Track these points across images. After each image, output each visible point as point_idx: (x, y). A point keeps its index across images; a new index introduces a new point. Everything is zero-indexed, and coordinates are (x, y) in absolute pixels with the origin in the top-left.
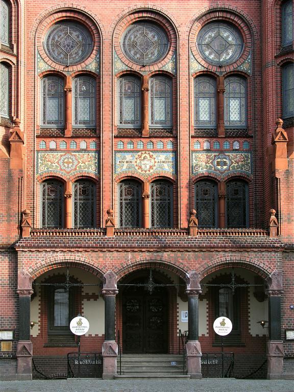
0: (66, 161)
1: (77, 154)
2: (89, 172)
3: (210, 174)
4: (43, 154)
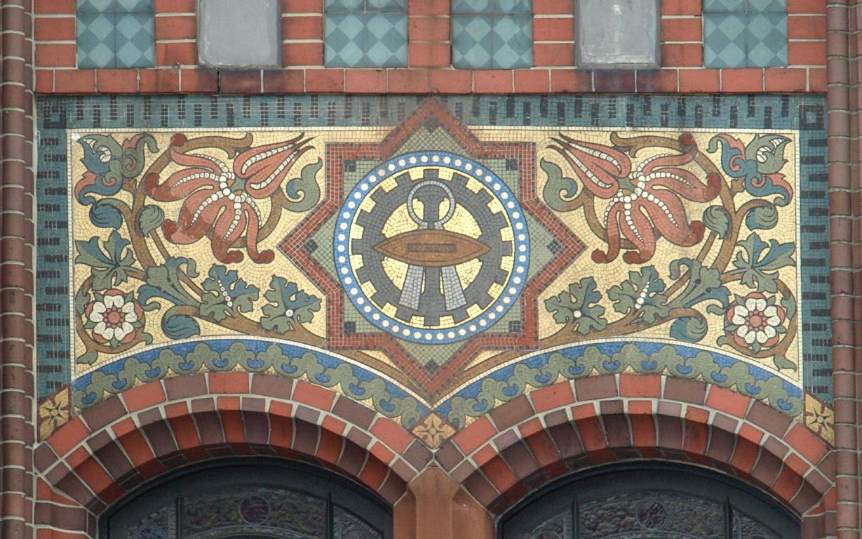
0: (399, 223)
1: (538, 135)
2: (702, 369)
4: (122, 134)
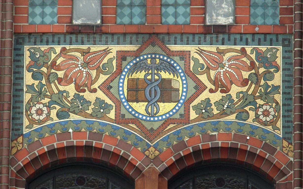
1: (192, 49)
3: (98, 136)
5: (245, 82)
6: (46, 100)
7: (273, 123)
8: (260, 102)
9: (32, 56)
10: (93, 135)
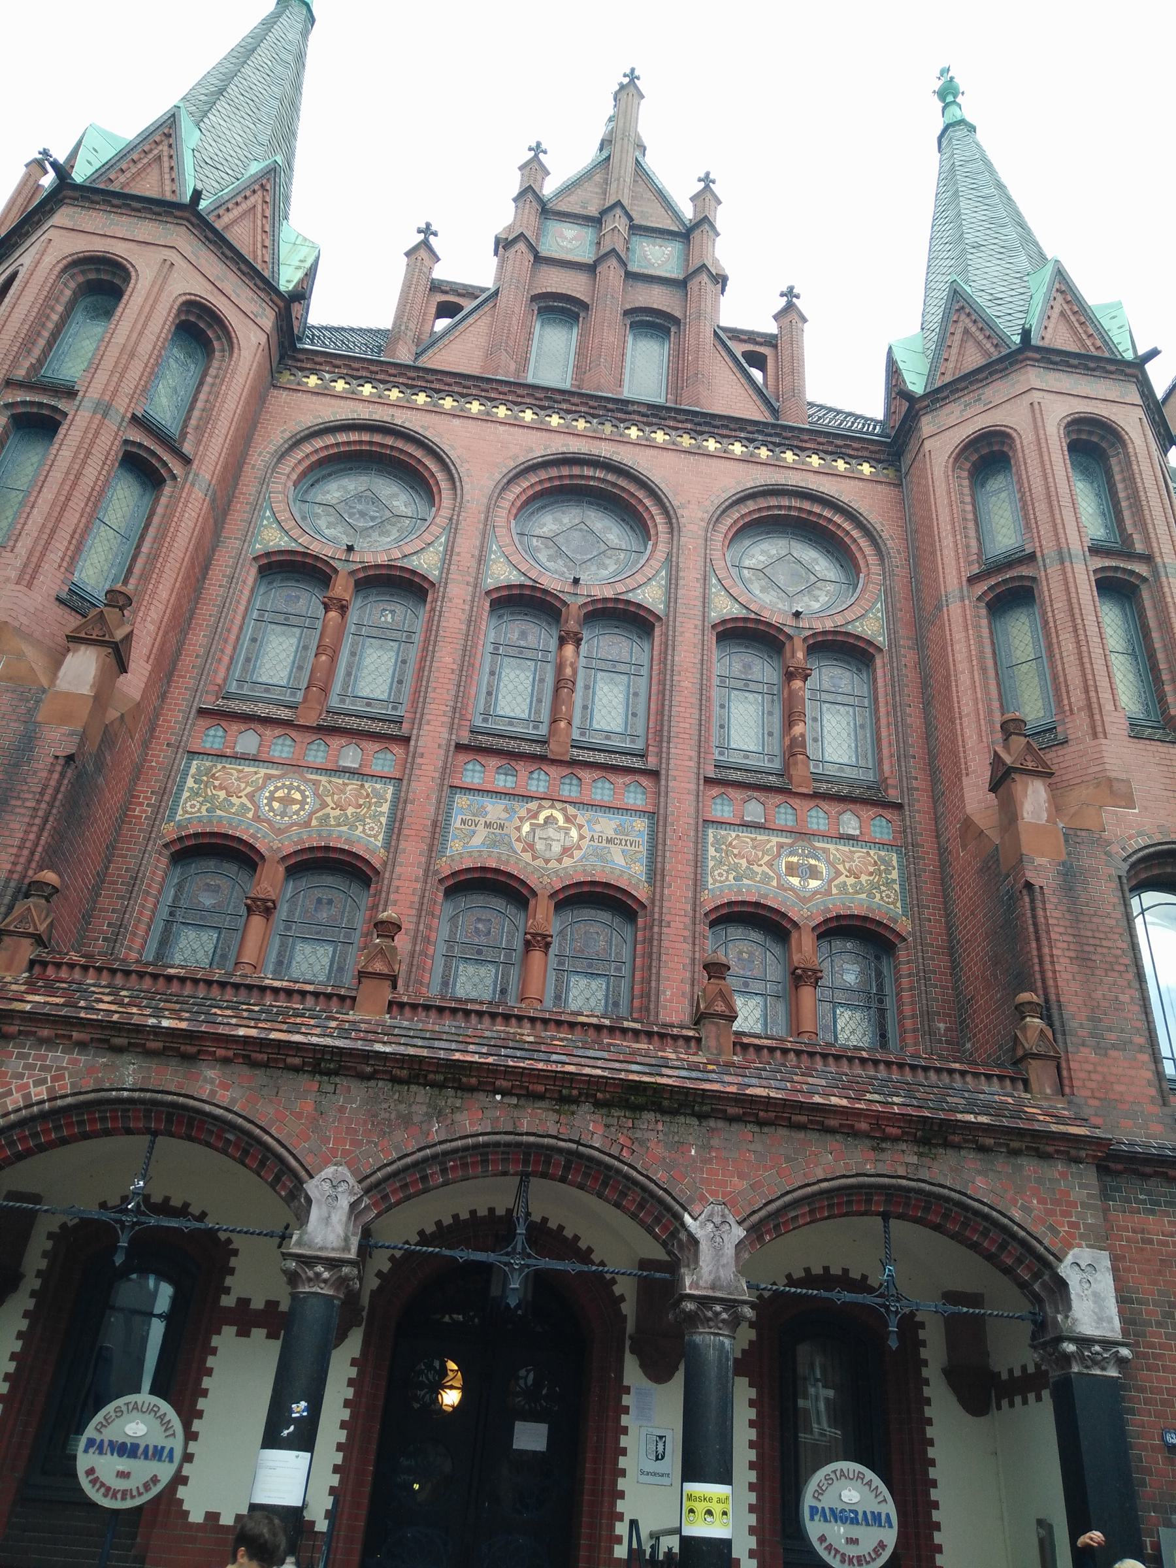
1: (831, 847)
3: (766, 896)
5: (871, 874)
6: (726, 868)
7: (375, 836)
8: (883, 888)
9: (198, 768)
10: (760, 895)
